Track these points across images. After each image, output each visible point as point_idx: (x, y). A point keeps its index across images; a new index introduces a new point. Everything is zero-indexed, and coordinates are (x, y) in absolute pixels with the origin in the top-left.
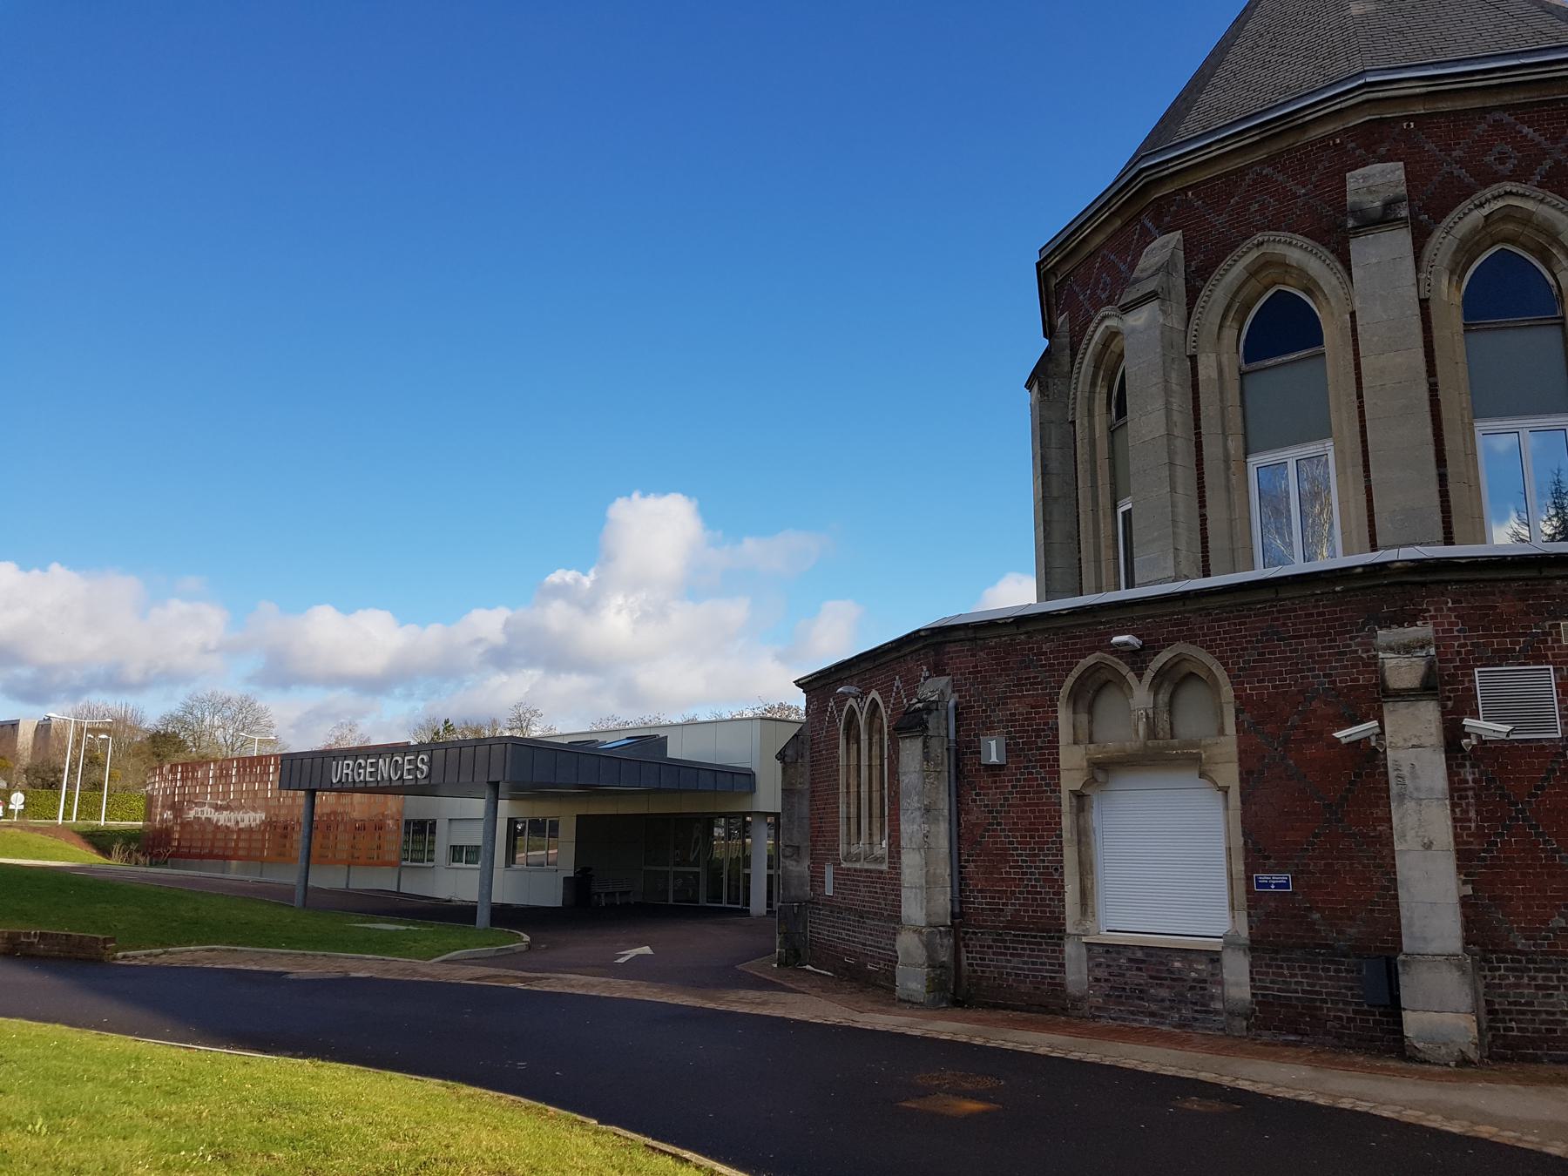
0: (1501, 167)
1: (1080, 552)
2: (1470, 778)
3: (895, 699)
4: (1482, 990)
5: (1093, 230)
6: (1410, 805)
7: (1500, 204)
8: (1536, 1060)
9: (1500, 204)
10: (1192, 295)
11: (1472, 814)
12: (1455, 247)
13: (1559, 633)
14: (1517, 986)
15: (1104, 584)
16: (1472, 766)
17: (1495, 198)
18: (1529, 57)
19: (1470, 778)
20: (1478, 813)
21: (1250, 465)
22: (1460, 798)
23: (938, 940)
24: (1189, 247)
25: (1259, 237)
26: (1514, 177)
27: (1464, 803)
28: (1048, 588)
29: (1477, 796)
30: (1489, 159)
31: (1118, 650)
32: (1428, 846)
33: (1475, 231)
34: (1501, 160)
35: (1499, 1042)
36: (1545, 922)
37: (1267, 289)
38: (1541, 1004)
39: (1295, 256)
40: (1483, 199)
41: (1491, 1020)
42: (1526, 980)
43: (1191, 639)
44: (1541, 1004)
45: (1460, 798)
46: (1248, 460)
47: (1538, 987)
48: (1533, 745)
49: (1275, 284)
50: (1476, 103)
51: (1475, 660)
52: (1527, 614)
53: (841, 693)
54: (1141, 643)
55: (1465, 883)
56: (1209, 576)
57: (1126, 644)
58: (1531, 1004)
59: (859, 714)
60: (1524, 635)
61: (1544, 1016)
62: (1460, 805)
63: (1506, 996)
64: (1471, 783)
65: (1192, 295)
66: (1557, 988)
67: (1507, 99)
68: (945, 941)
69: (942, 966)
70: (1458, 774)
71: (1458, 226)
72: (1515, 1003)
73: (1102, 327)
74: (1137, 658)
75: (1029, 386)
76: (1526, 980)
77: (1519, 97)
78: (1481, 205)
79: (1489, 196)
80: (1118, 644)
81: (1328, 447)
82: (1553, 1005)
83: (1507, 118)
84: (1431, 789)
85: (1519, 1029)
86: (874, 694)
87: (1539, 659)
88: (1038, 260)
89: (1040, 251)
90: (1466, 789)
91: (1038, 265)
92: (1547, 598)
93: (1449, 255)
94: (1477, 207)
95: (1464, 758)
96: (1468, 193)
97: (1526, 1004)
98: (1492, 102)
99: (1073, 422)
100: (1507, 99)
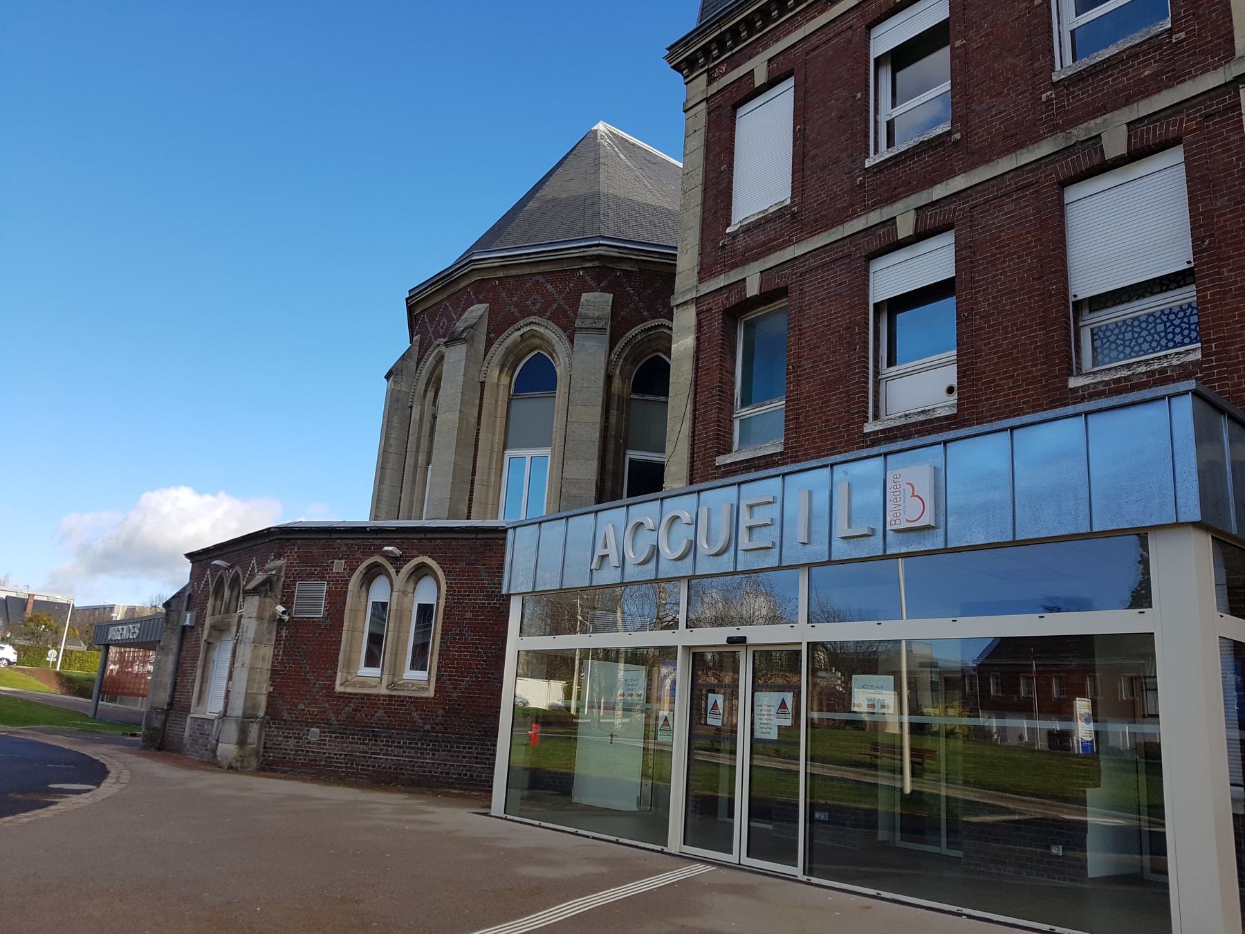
0: (534, 307)
1: (401, 493)
2: (284, 635)
3: (250, 572)
4: (263, 736)
5: (443, 286)
6: (243, 645)
7: (528, 328)
8: (276, 771)
9: (528, 328)
10: (489, 344)
11: (281, 653)
12: (503, 352)
13: (333, 566)
14: (276, 736)
15: (413, 515)
16: (286, 630)
17: (526, 325)
18: (528, 249)
19: (284, 635)
20: (283, 652)
21: (506, 455)
22: (278, 644)
23: (154, 715)
24: (492, 312)
25: (532, 319)
26: (540, 313)
27: (279, 646)
28: (375, 515)
29: (285, 644)
30: (529, 303)
31: (387, 555)
32: (243, 665)
33: (516, 345)
34: (534, 303)
35: (265, 762)
36: (296, 706)
37: (531, 351)
38: (284, 745)
39: (548, 334)
40: (519, 326)
41: (264, 752)
42: (281, 733)
43: (424, 554)
44: (284, 745)
45: (278, 644)
46: (506, 452)
47: (284, 737)
48: (316, 620)
49: (541, 349)
50: (527, 271)
51: (299, 577)
52: (323, 556)
53: (215, 565)
54: (401, 553)
55: (271, 685)
56: (470, 519)
57: (391, 552)
58: (280, 745)
59: (225, 581)
60: (320, 566)
61: (284, 751)
62: (277, 648)
63: (272, 740)
64: (284, 638)
65: (489, 344)
66: (291, 737)
67: (542, 269)
68: (159, 717)
69: (154, 729)
70: (280, 633)
71: (507, 341)
72: (275, 744)
73: (436, 351)
74: (398, 562)
75: (387, 377)
76: (281, 733)
77: (547, 268)
78: (519, 329)
79: (522, 324)
80: (387, 551)
81: (547, 451)
82: (288, 746)
83: (541, 279)
84: (249, 638)
85: (274, 757)
86: (238, 568)
87: (322, 578)
88: (408, 296)
89: (410, 291)
90: (281, 641)
91: (407, 299)
92: (333, 548)
93: (500, 356)
94: (516, 330)
95: (284, 625)
96: (516, 320)
97: (278, 745)
98: (534, 270)
99: (411, 407)
100: (542, 269)
